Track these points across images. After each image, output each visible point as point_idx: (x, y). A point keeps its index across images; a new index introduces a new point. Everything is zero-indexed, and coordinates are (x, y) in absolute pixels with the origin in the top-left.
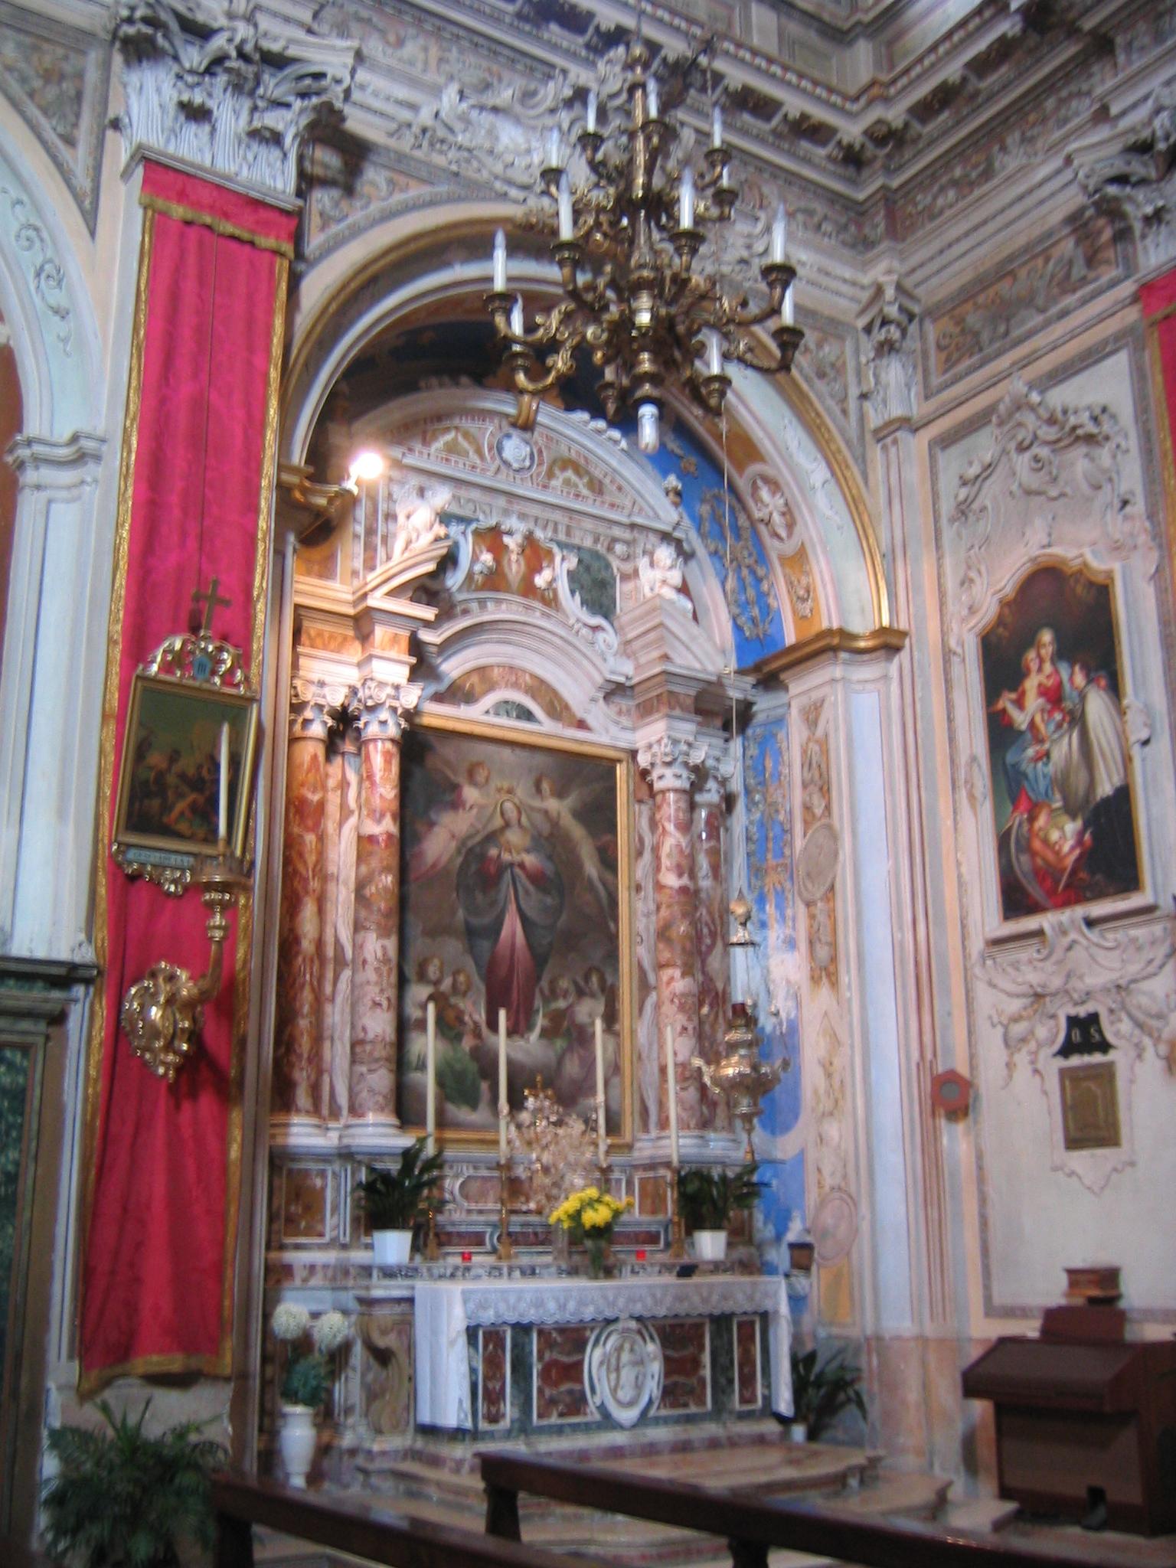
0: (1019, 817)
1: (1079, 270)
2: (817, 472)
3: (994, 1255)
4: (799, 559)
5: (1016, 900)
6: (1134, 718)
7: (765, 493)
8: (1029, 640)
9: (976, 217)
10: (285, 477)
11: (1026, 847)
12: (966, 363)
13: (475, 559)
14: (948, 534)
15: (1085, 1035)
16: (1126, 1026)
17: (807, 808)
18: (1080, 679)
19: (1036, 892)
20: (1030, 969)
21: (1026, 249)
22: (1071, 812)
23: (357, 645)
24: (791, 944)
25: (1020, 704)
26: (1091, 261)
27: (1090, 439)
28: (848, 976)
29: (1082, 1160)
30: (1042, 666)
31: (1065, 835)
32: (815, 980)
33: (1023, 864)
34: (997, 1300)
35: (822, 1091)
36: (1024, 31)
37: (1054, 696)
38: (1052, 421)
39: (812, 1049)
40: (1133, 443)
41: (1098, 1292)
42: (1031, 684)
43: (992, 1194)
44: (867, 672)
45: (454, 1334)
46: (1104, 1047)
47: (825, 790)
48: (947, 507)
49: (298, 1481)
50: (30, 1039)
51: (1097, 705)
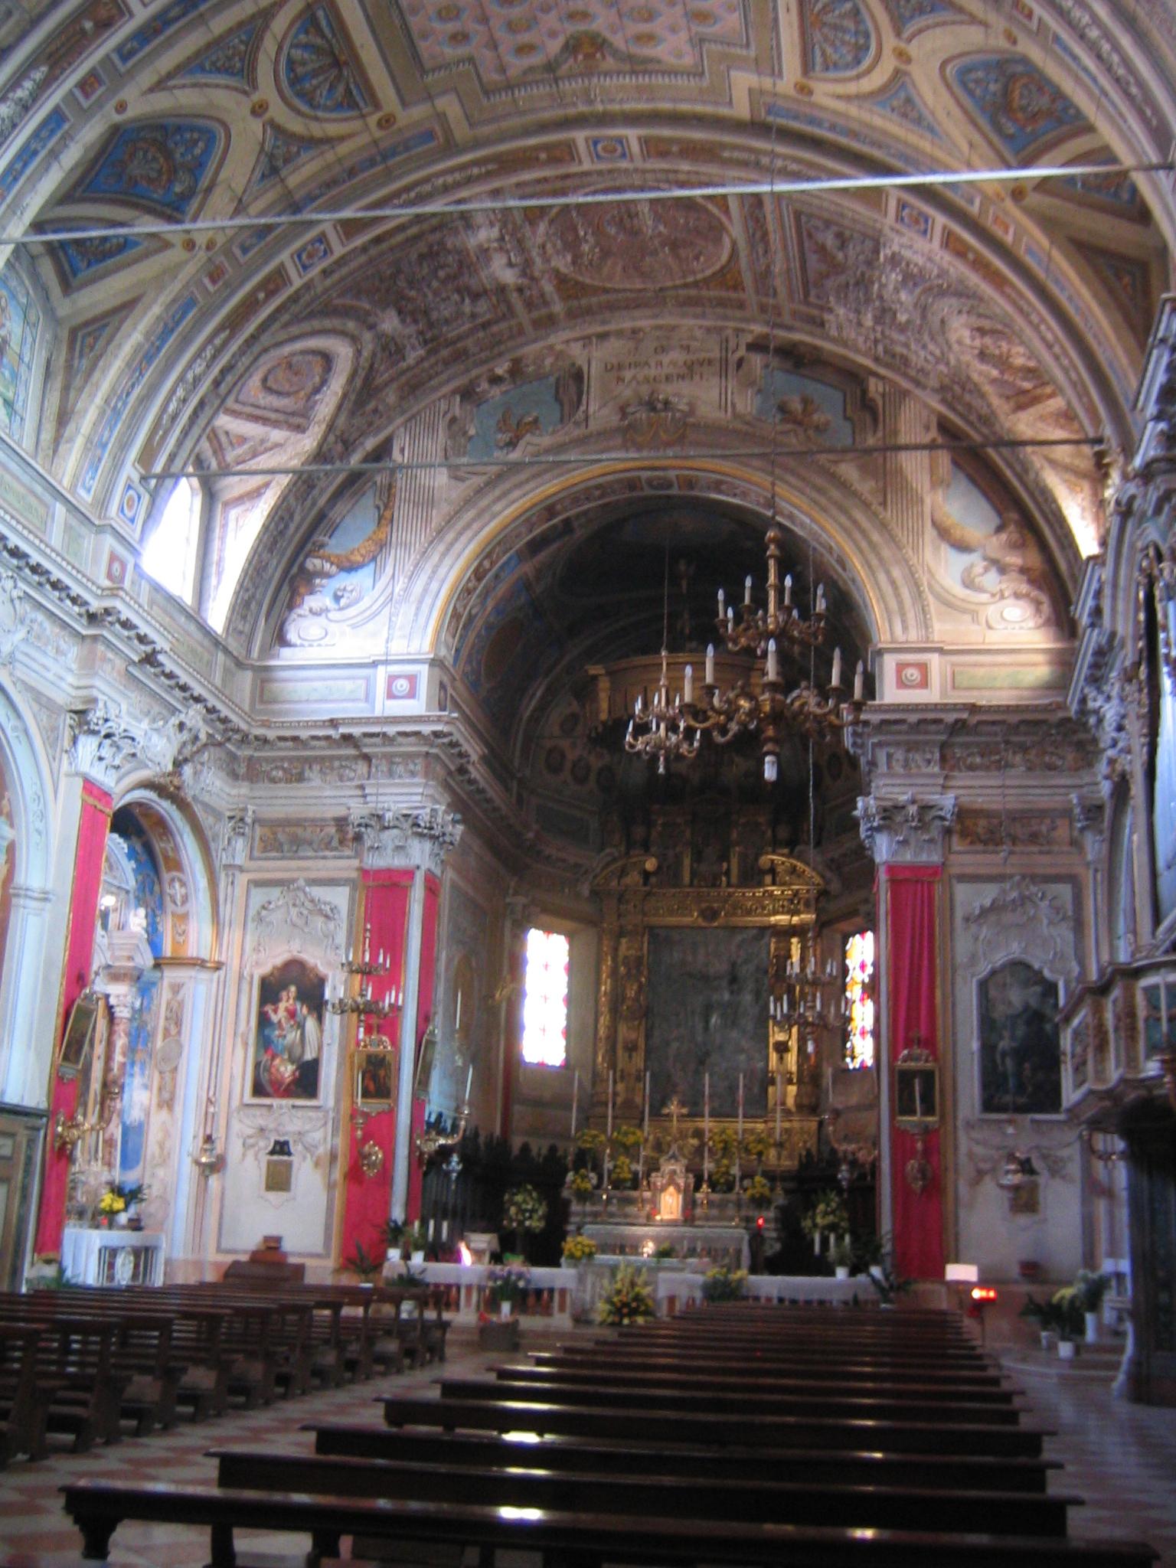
0: (265, 1058)
1: (335, 843)
2: (202, 882)
3: (225, 1227)
4: (184, 917)
5: (258, 1090)
6: (326, 1034)
7: (177, 885)
8: (285, 987)
11: (268, 1070)
12: (274, 854)
14: (251, 925)
15: (281, 1148)
16: (300, 1147)
17: (167, 1031)
18: (305, 1010)
19: (269, 1089)
20: (261, 1119)
21: (313, 820)
22: (291, 1060)
24: (146, 1087)
25: (275, 1011)
26: (341, 842)
27: (327, 916)
28: (178, 1108)
29: (274, 1196)
30: (288, 999)
31: (287, 1071)
32: (160, 1106)
33: (265, 1077)
34: (223, 1245)
37: (292, 1014)
38: (312, 901)
39: (153, 1136)
40: (345, 926)
41: (272, 1245)
42: (282, 1005)
43: (227, 1203)
44: (204, 975)
46: (289, 1154)
47: (178, 1023)
48: (252, 912)
51: (311, 1024)
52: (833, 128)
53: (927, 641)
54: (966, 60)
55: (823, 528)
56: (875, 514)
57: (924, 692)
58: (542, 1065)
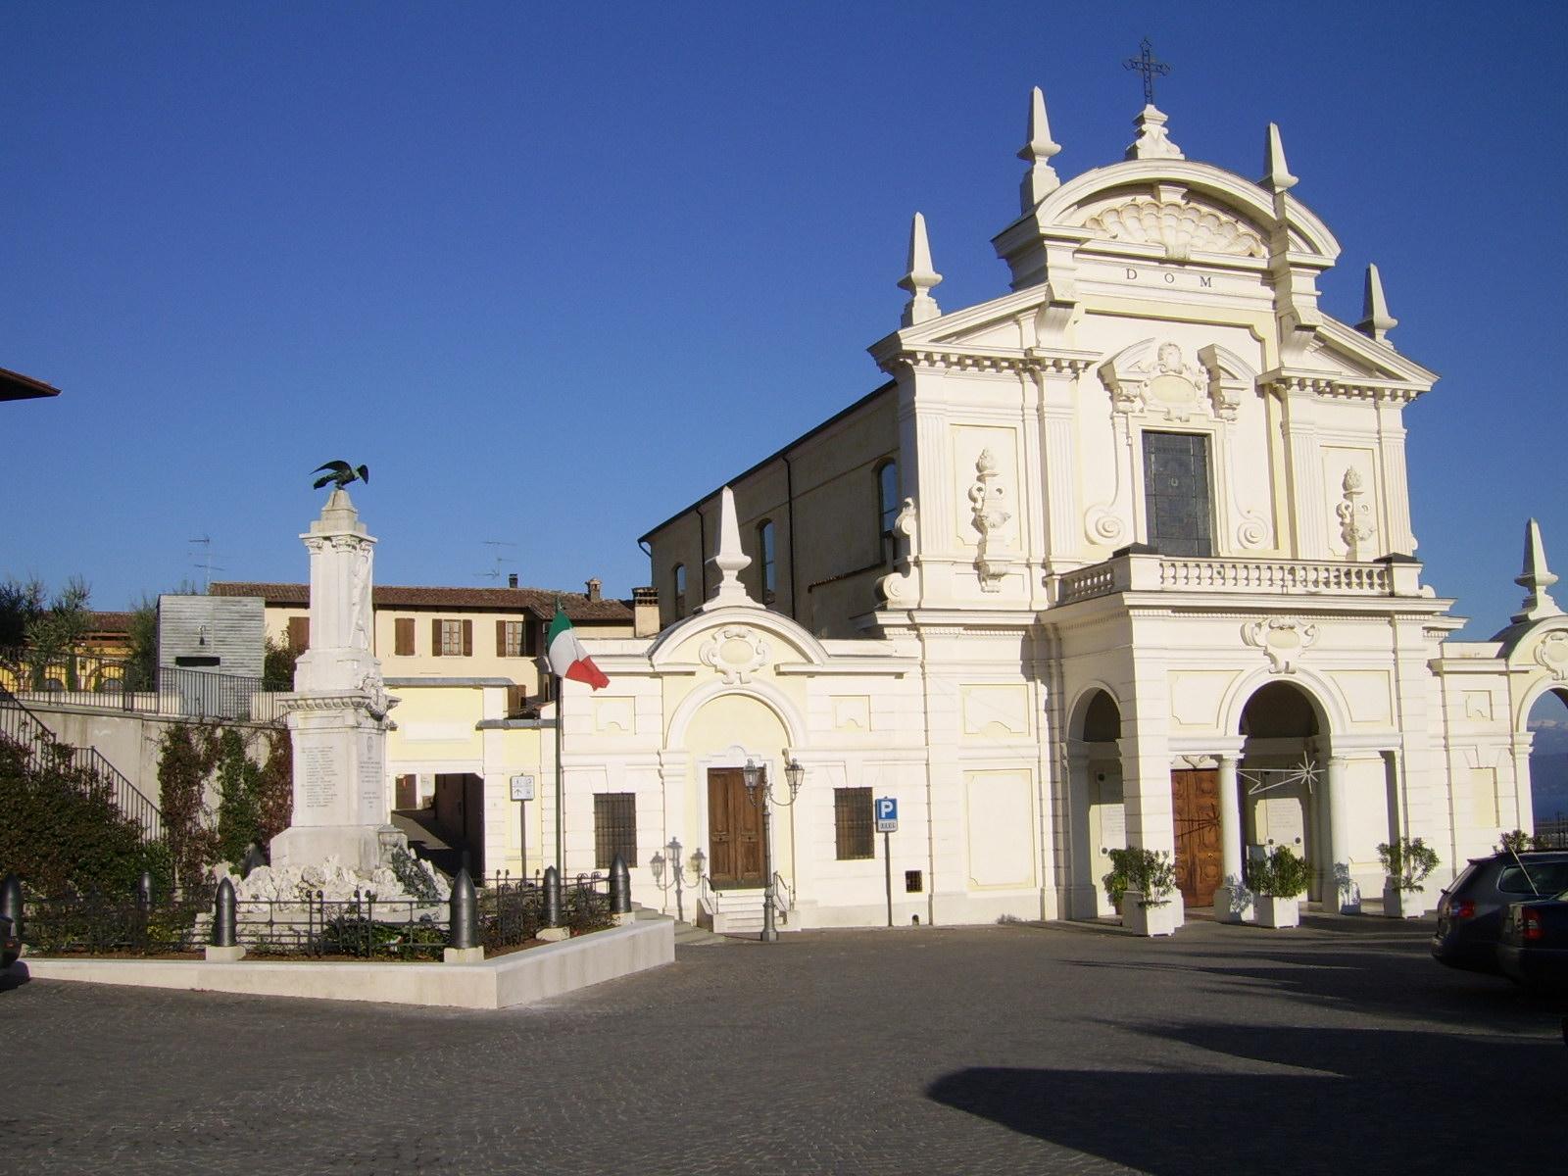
9: (745, 923)
10: (79, 751)
13: (394, 945)
23: (703, 861)
35: (372, 858)
36: (1030, 145)
45: (1282, 656)
49: (1273, 215)
50: (733, 872)
52: (903, 664)
53: (84, 724)
54: (1398, 761)
55: (1071, 706)
56: (169, 722)
57: (1130, 165)
58: (1008, 924)
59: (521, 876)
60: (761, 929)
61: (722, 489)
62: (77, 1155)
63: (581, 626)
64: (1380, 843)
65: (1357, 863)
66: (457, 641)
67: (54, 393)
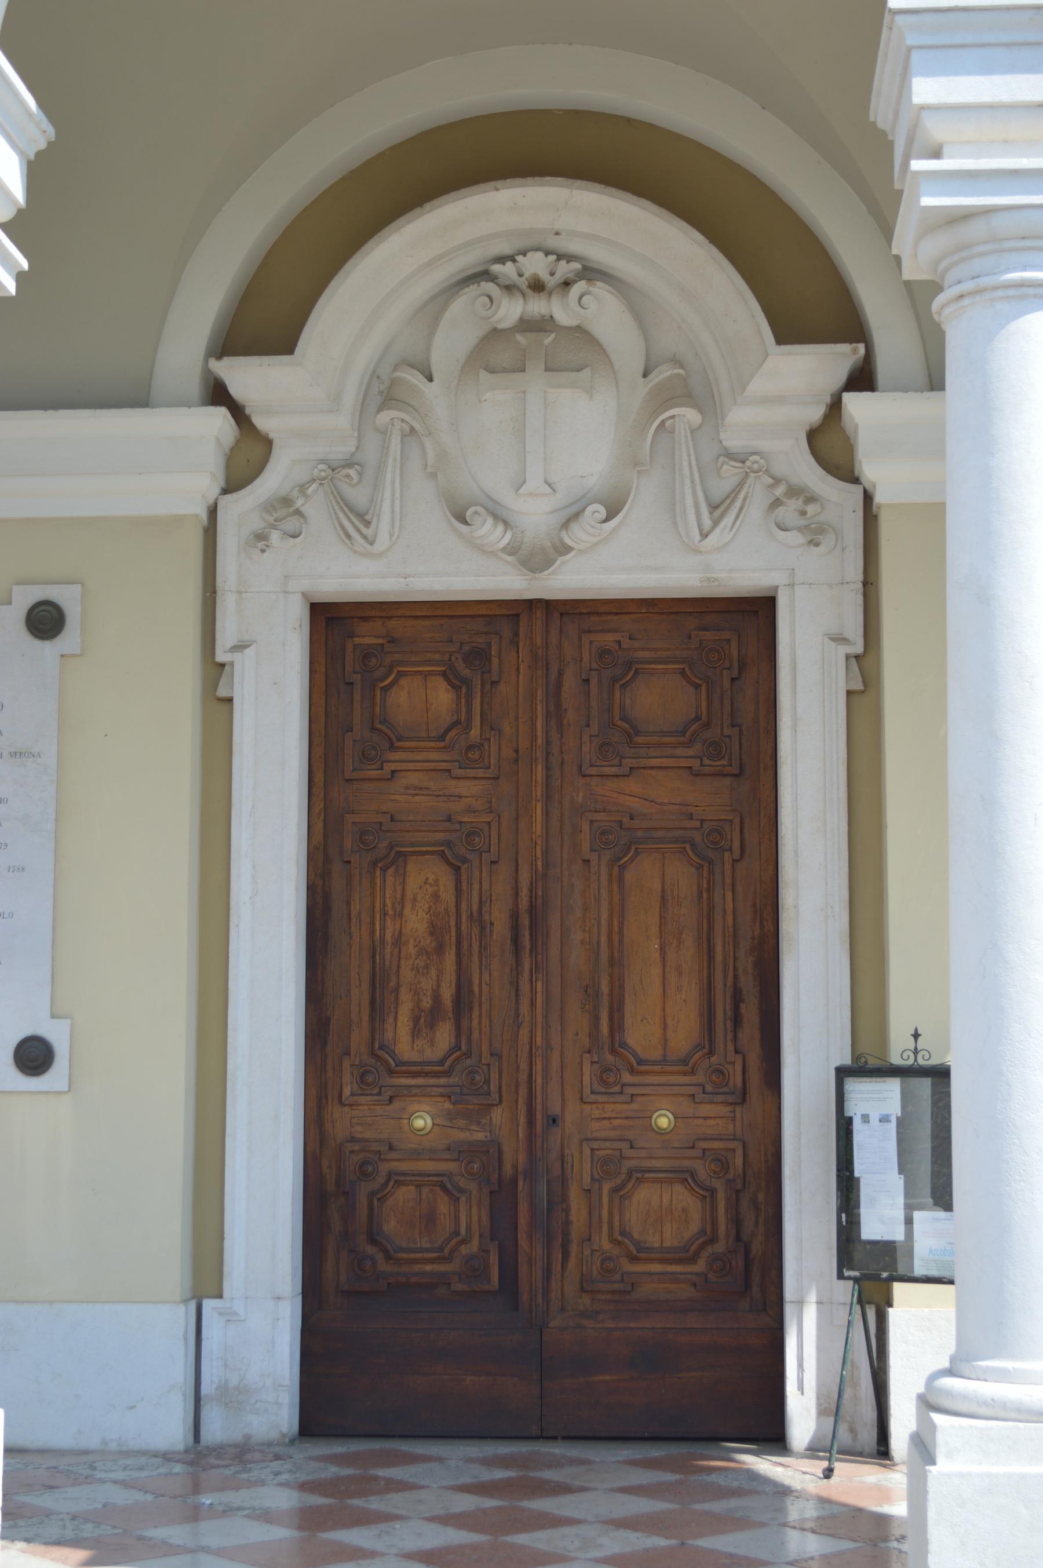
59: (851, 1282)
60: (851, 1282)
61: (835, 407)
62: (391, 1100)
63: (839, 1188)
64: (914, 1396)
65: (625, 829)
66: (727, 665)
67: (802, 1394)
